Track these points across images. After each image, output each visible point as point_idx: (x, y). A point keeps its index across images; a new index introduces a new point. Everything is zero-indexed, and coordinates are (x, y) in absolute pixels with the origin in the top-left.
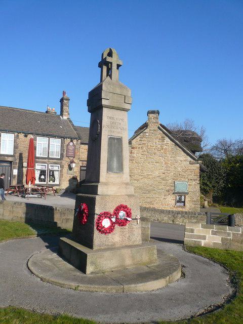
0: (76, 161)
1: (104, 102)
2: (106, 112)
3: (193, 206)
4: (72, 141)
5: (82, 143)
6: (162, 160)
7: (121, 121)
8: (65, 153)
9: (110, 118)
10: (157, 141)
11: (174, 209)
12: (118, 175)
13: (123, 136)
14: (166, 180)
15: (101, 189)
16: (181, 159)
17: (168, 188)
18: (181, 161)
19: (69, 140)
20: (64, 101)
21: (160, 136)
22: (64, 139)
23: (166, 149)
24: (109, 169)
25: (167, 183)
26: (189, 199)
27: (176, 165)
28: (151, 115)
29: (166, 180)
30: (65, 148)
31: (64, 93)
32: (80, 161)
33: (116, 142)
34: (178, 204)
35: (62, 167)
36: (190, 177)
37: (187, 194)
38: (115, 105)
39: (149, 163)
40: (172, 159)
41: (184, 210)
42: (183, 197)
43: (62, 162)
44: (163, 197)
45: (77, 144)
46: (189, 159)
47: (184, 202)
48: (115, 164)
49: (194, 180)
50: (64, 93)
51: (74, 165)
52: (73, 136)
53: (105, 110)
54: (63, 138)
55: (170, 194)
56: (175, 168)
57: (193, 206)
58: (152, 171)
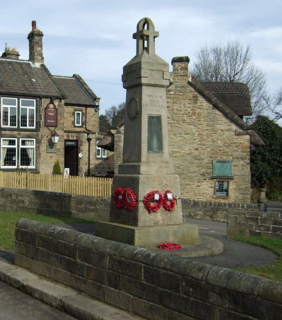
0: (59, 132)
1: (144, 81)
2: (145, 91)
3: (240, 196)
4: (52, 102)
5: (66, 104)
6: (194, 131)
7: (159, 99)
8: (43, 120)
9: (149, 96)
10: (187, 102)
11: (213, 201)
12: (157, 154)
13: (162, 115)
14: (200, 159)
15: (143, 169)
16: (222, 127)
17: (203, 170)
18: (222, 130)
19: (48, 101)
20: (36, 37)
21: (190, 95)
22: (41, 99)
23: (199, 114)
24: (150, 148)
25: (201, 163)
26: (235, 187)
27: (215, 136)
28: (177, 64)
29: (200, 159)
30: (43, 114)
31: (34, 24)
32: (65, 132)
33: (155, 121)
34: (218, 194)
35: (38, 142)
36: (236, 154)
37: (232, 178)
38: (152, 83)
39: (175, 135)
40: (209, 128)
41: (226, 202)
42: (225, 184)
43: (38, 135)
44: (196, 184)
45: (59, 106)
46: (234, 127)
47: (227, 191)
48: (155, 143)
49: (242, 159)
50: (34, 24)
51: (56, 139)
52: (54, 94)
53: (144, 88)
54: (39, 97)
55: (205, 179)
56: (214, 141)
57: (240, 196)
58: (179, 147)
